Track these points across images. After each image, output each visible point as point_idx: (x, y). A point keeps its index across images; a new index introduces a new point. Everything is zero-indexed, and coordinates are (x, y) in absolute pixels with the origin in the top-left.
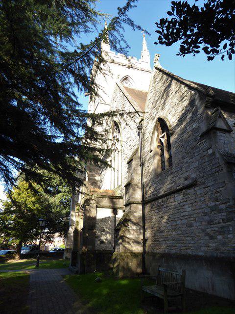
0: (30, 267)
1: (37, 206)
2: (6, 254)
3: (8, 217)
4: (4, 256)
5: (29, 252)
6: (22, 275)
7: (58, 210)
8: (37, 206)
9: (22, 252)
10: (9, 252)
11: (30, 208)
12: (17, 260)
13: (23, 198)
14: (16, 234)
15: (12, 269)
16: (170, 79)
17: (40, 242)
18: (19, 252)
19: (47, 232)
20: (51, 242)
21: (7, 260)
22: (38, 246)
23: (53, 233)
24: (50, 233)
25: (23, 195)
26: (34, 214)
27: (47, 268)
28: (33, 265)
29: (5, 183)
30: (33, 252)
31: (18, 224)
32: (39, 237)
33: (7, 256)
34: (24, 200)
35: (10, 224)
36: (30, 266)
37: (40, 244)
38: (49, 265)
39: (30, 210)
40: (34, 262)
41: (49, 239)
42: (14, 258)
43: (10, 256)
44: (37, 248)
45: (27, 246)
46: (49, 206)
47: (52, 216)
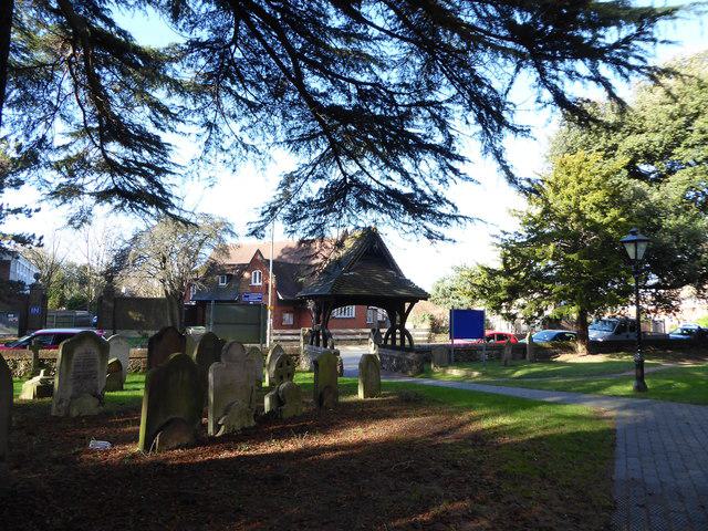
0: (616, 389)
1: (614, 212)
2: (555, 338)
3: (539, 252)
4: (547, 345)
5: (610, 336)
6: (585, 427)
7: (682, 219)
8: (614, 212)
9: (593, 335)
10: (561, 336)
11: (591, 221)
12: (580, 357)
13: (569, 197)
14: (565, 290)
15: (564, 389)
16: (633, 373)
17: (640, 311)
18: (582, 336)
19: (657, 286)
20: (670, 309)
21: (556, 354)
22: (632, 321)
23: (674, 287)
24: (665, 288)
25: (569, 190)
26: (609, 238)
27: (676, 397)
28: (624, 381)
29: (479, 128)
30: (622, 337)
31: (567, 267)
32: (632, 298)
33: (556, 346)
34: (572, 203)
35: (549, 269)
36: (616, 383)
37: (638, 315)
38: (684, 386)
39: (596, 228)
40: (626, 366)
41: (667, 305)
42: (572, 350)
43: (562, 343)
44: (625, 326)
45: (605, 322)
46: (653, 211)
47: (667, 239)
